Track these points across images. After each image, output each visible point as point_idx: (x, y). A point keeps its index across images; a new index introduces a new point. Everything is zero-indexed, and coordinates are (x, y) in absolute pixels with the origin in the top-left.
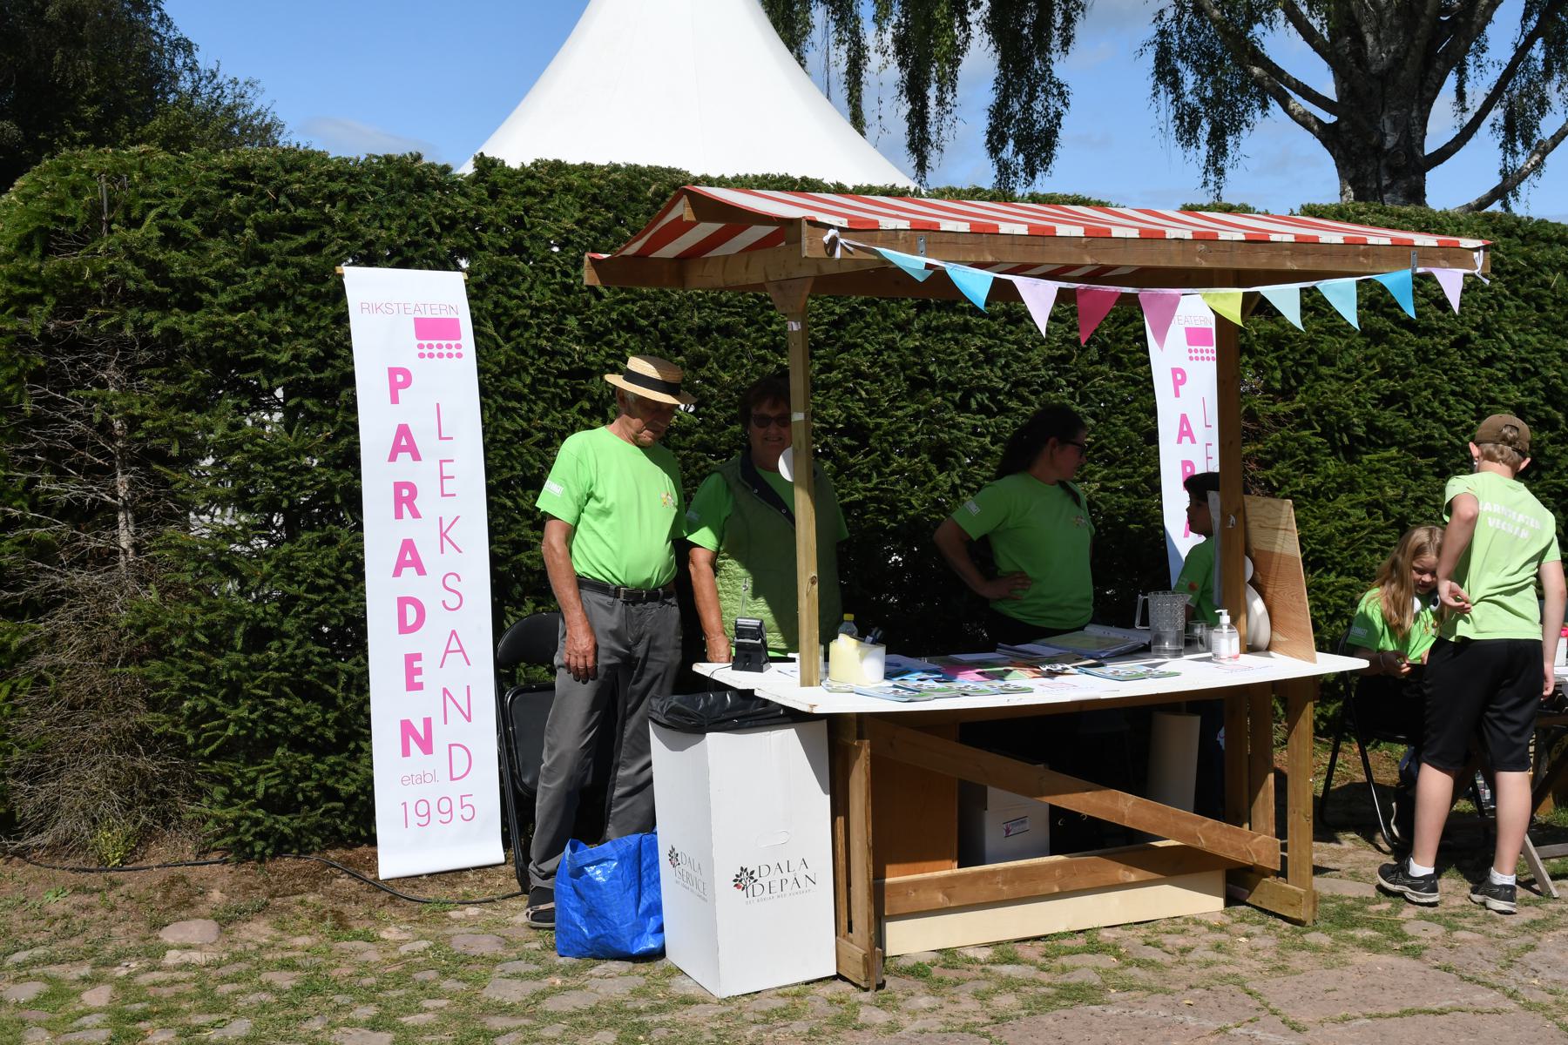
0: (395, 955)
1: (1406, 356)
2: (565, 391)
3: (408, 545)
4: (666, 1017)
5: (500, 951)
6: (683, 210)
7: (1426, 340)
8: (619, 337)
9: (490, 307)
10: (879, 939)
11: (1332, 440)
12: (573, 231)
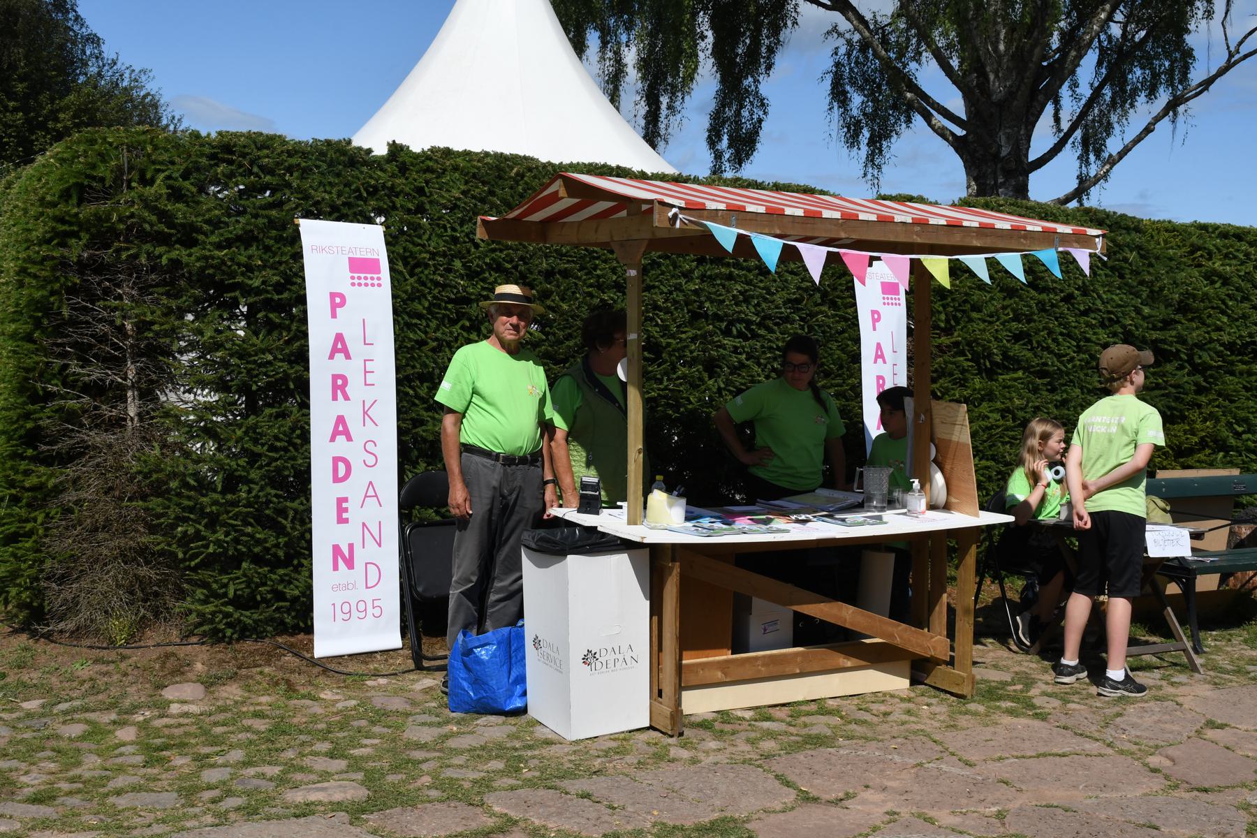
0: (335, 710)
1: (1030, 307)
2: (452, 313)
3: (341, 420)
4: (537, 752)
5: (408, 708)
6: (557, 186)
7: (1044, 296)
8: (491, 276)
9: (401, 251)
10: (678, 702)
11: (978, 363)
12: (459, 199)
